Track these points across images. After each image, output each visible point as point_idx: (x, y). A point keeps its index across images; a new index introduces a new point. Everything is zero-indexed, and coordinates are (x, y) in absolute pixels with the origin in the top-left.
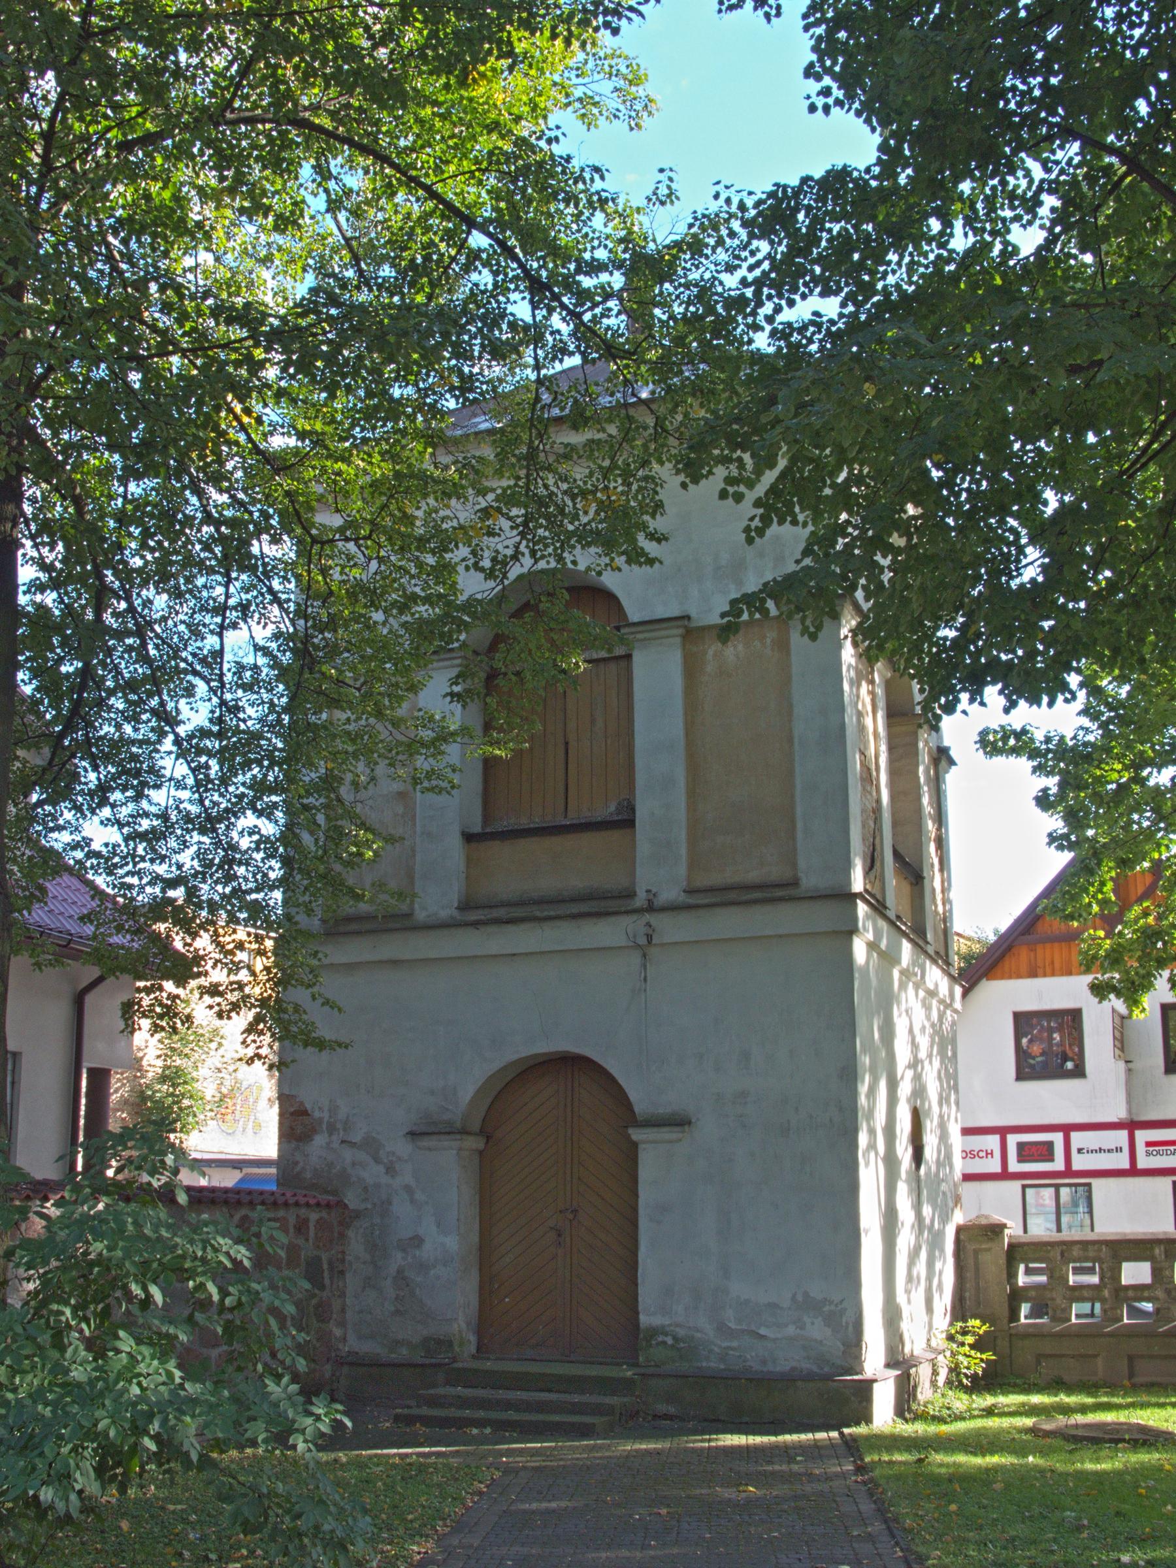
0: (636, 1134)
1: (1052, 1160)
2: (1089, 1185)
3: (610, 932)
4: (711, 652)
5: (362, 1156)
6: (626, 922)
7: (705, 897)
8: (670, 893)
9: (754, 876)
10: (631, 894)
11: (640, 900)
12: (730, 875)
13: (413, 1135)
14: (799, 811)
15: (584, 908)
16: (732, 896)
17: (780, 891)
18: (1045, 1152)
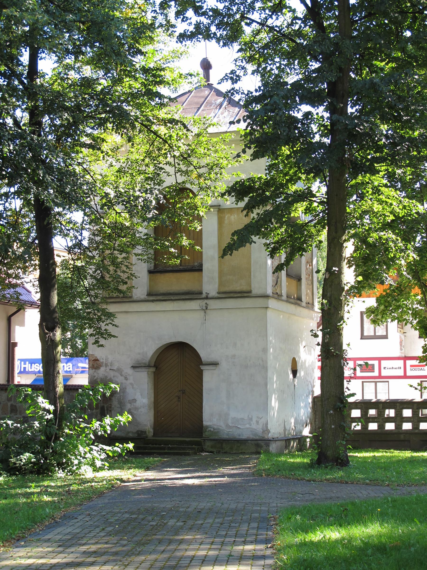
0: (202, 367)
1: (374, 372)
2: (388, 382)
3: (194, 305)
4: (227, 217)
5: (117, 374)
6: (199, 302)
7: (226, 295)
8: (213, 294)
9: (238, 289)
10: (201, 293)
11: (204, 295)
12: (232, 288)
13: (134, 367)
14: (252, 270)
15: (187, 297)
16: (232, 295)
17: (245, 294)
18: (371, 368)
